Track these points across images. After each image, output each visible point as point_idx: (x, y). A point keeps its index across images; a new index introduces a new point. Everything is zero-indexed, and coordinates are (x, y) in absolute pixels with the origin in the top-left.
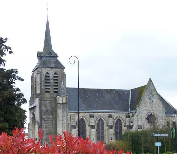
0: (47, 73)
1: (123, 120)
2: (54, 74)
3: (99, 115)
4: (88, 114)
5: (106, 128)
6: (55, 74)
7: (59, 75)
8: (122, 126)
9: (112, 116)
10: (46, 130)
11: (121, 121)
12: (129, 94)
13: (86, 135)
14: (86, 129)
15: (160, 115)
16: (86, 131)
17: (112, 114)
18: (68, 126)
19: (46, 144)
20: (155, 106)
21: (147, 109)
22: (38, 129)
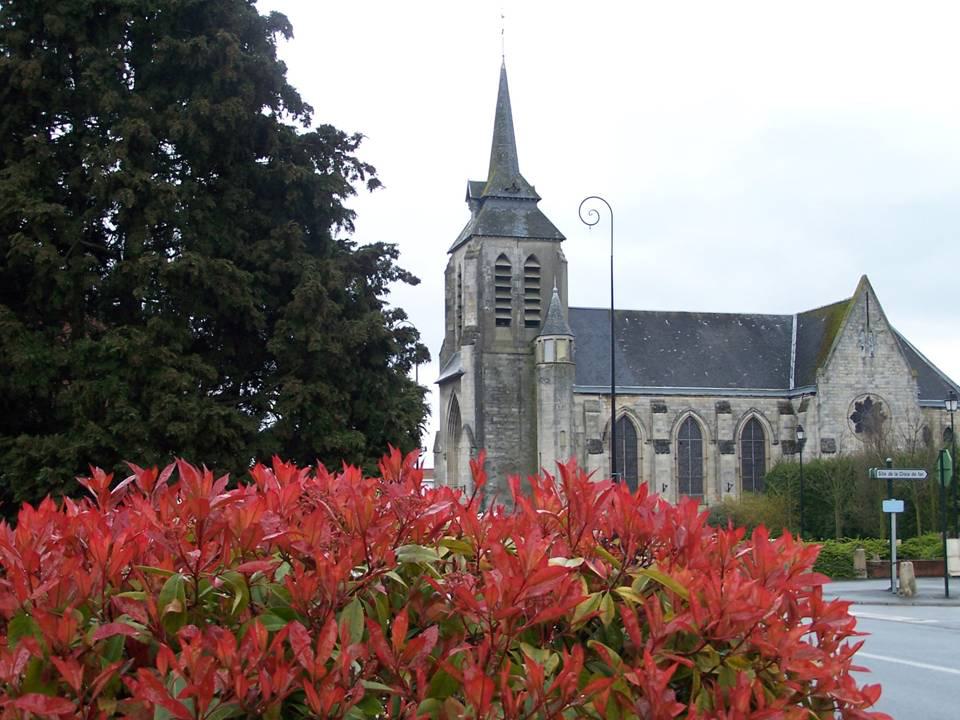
1: (769, 422)
3: (683, 405)
4: (646, 401)
5: (709, 449)
6: (531, 258)
7: (543, 263)
9: (729, 407)
14: (639, 451)
15: (900, 403)
16: (639, 461)
17: (731, 401)
20: (882, 373)
21: (853, 383)
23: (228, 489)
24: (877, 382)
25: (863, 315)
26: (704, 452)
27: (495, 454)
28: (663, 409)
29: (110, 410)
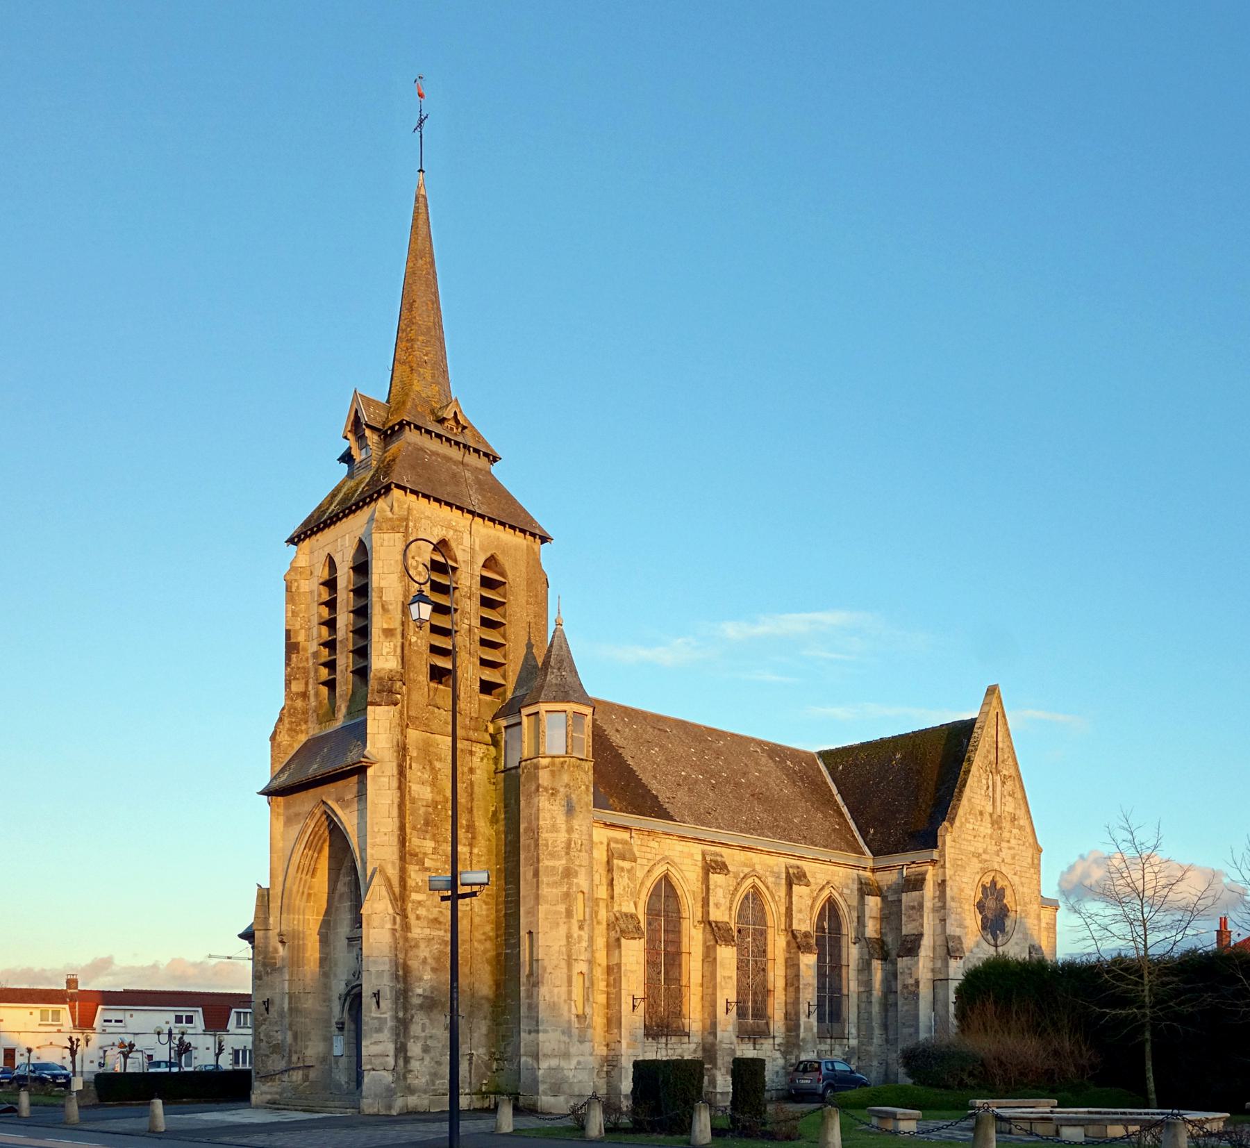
0: (442, 546)
1: (849, 906)
2: (481, 561)
3: (745, 865)
4: (697, 849)
5: (694, 939)
6: (491, 562)
7: (515, 575)
8: (844, 940)
9: (805, 876)
10: (429, 940)
11: (841, 913)
12: (826, 783)
13: (684, 982)
14: (685, 940)
15: (1025, 890)
16: (684, 957)
17: (807, 866)
18: (594, 913)
19: (566, 762)
20: (1009, 841)
21: (981, 851)
22: (389, 926)
23: (386, 457)
24: (1003, 854)
25: (1003, 762)
26: (770, 948)
27: (427, 931)
28: (722, 868)
29: (866, 1112)
